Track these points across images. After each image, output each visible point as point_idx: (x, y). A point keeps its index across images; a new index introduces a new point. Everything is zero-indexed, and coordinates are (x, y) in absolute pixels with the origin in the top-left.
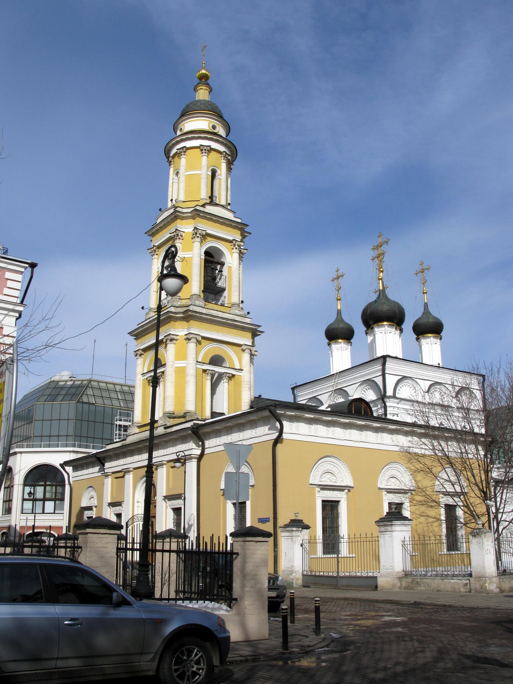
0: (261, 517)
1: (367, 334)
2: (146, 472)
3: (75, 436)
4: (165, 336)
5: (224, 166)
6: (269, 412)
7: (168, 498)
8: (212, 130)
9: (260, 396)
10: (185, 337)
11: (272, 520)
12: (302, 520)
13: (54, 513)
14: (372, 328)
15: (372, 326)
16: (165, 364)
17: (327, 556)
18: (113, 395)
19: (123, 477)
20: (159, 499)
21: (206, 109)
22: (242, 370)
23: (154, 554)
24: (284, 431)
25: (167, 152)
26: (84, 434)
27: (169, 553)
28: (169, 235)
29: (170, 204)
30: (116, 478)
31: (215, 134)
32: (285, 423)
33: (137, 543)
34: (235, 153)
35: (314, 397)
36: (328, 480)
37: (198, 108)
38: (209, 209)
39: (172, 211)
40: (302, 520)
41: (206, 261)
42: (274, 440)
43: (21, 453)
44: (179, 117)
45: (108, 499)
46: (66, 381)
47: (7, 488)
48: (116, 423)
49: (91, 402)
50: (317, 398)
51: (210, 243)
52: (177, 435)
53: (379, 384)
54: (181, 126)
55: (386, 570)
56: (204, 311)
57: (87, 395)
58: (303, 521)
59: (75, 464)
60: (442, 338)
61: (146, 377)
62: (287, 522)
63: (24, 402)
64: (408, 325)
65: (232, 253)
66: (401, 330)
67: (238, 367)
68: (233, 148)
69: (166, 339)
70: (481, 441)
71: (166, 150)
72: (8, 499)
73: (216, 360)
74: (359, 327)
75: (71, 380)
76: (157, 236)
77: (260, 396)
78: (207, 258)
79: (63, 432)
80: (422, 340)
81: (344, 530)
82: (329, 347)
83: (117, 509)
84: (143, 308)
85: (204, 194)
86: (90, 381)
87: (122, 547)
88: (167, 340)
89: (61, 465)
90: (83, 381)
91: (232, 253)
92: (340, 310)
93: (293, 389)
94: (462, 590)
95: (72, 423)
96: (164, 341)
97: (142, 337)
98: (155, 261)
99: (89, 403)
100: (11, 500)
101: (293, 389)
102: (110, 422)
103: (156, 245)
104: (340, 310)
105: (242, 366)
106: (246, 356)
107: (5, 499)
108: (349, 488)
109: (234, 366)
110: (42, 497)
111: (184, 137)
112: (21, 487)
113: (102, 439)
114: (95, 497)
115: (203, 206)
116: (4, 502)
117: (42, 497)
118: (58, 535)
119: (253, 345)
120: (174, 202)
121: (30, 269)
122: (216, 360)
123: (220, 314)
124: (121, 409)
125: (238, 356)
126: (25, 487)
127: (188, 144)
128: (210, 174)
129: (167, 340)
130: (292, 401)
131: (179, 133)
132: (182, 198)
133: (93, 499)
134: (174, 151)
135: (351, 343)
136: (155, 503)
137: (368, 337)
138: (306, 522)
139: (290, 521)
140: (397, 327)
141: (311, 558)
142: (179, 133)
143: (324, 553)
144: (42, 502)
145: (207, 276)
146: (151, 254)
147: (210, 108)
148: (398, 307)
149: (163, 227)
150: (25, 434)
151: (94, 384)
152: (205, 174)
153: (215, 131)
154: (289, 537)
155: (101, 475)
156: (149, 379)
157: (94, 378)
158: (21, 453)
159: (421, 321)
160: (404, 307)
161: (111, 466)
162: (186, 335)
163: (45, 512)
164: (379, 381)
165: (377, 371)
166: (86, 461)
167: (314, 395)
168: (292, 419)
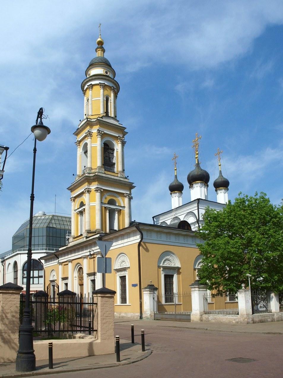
0: (133, 284)
1: (190, 188)
3: (47, 244)
4: (85, 189)
5: (112, 95)
7: (89, 275)
8: (105, 74)
9: (135, 221)
10: (95, 189)
11: (138, 285)
12: (154, 285)
13: (38, 284)
14: (193, 184)
16: (85, 204)
18: (65, 223)
19: (68, 264)
22: (125, 207)
23: (47, 304)
25: (82, 87)
26: (51, 243)
28: (85, 134)
29: (85, 117)
30: (64, 265)
33: (57, 298)
34: (119, 87)
35: (164, 222)
36: (168, 264)
38: (105, 120)
39: (86, 120)
40: (154, 285)
42: (138, 243)
43: (20, 254)
45: (61, 276)
47: (15, 272)
48: (67, 237)
51: (106, 139)
52: (92, 241)
54: (89, 72)
55: (195, 311)
56: (104, 175)
57: (52, 223)
58: (154, 286)
61: (76, 212)
62: (146, 286)
63: (21, 228)
64: (211, 183)
65: (118, 144)
66: (208, 186)
67: (122, 205)
69: (85, 191)
72: (16, 277)
74: (186, 184)
75: (44, 216)
77: (135, 221)
78: (105, 146)
81: (175, 290)
82: (171, 195)
83: (66, 281)
84: (73, 175)
86: (53, 216)
87: (57, 302)
89: (39, 259)
90: (49, 216)
91: (118, 144)
92: (176, 175)
93: (153, 218)
94: (234, 322)
95: (45, 238)
96: (84, 192)
97: (74, 191)
98: (78, 149)
99: (53, 228)
100: (17, 278)
101: (153, 218)
103: (79, 140)
104: (176, 175)
106: (126, 200)
107: (15, 278)
108: (179, 269)
109: (121, 204)
110: (34, 279)
111: (90, 79)
112: (21, 271)
113: (56, 245)
114: (55, 275)
115: (102, 118)
116: (14, 279)
117: (34, 279)
118: (233, 298)
119: (130, 194)
120: (87, 115)
121: (5, 151)
122: (112, 202)
123: (113, 177)
125: (122, 200)
126: (94, 279)
127: (93, 83)
128: (105, 99)
130: (153, 224)
132: (90, 113)
133: (55, 276)
134: (86, 87)
135: (182, 193)
136: (83, 277)
137: (191, 189)
138: (156, 286)
140: (205, 184)
141: (225, 303)
144: (37, 279)
146: (77, 145)
147: (104, 61)
148: (205, 172)
150: (22, 245)
151: (56, 218)
152: (101, 99)
153: (108, 75)
154: (147, 294)
156: (78, 213)
158: (20, 254)
160: (209, 173)
162: (95, 188)
163: (34, 283)
164: (196, 212)
165: (195, 207)
167: (164, 221)
168: (148, 231)
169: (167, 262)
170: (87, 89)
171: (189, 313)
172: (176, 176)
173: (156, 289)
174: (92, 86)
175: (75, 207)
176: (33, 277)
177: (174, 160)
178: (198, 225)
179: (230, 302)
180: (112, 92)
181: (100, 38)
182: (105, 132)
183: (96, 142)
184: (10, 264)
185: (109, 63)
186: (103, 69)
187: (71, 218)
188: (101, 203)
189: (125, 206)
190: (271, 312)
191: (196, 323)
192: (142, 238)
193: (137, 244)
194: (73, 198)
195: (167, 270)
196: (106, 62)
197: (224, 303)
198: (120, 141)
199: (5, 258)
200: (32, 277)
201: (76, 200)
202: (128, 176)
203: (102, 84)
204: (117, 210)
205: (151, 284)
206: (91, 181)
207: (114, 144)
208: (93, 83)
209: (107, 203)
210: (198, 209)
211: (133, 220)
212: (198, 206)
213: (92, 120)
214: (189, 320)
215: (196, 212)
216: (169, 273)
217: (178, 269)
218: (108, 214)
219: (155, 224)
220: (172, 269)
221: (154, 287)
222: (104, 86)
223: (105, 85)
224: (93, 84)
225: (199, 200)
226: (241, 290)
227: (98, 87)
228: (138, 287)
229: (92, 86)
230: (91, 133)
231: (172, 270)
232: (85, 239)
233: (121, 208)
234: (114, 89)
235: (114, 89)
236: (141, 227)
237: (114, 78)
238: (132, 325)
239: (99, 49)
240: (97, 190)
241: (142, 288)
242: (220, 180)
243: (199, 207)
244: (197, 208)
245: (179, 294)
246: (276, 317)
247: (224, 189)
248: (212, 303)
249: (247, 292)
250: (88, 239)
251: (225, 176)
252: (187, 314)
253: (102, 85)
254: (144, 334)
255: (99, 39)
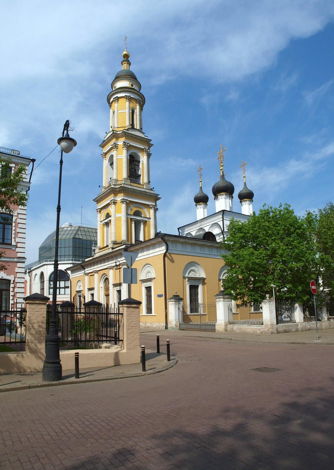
0: (159, 294)
1: (215, 199)
2: (58, 268)
4: (111, 201)
5: (138, 107)
6: (161, 239)
7: (115, 285)
9: (160, 232)
10: (121, 201)
12: (179, 296)
13: (65, 294)
14: (217, 196)
15: (217, 195)
16: (111, 216)
17: (256, 312)
19: (94, 275)
20: (111, 286)
21: (127, 74)
22: (151, 218)
24: (169, 249)
25: (108, 100)
27: (91, 312)
28: (111, 146)
29: (111, 129)
31: (133, 89)
32: (170, 245)
36: (193, 275)
37: (123, 74)
39: (112, 132)
40: (179, 296)
41: (130, 160)
43: (47, 265)
44: (114, 79)
45: (87, 287)
46: (67, 228)
48: (93, 248)
49: (80, 238)
50: (190, 233)
51: (132, 151)
53: (221, 226)
56: (130, 187)
59: (71, 269)
60: (253, 201)
61: (102, 223)
66: (232, 197)
67: (148, 216)
68: (143, 97)
70: (318, 265)
71: (108, 98)
73: (137, 213)
74: (211, 196)
75: (70, 227)
76: (105, 148)
77: (160, 232)
79: (67, 254)
80: (243, 202)
81: (200, 301)
83: (92, 292)
84: (99, 186)
85: (127, 124)
88: (111, 203)
90: (76, 227)
91: (143, 156)
92: (201, 187)
93: (178, 229)
95: (71, 249)
98: (104, 161)
99: (79, 239)
101: (178, 229)
102: (90, 248)
104: (201, 187)
105: (151, 216)
107: (41, 288)
108: (204, 279)
110: (61, 289)
111: (116, 91)
112: (48, 282)
114: (82, 286)
115: (127, 130)
116: (41, 289)
117: (61, 289)
118: (258, 308)
119: (156, 205)
120: (113, 127)
121: (32, 163)
122: (137, 213)
123: (138, 189)
124: (95, 241)
125: (148, 211)
127: (119, 95)
128: (131, 112)
129: (111, 203)
131: (114, 89)
132: (116, 126)
134: (112, 99)
135: (207, 204)
136: (109, 288)
138: (181, 296)
139: (172, 296)
140: (230, 195)
142: (114, 89)
143: (191, 312)
145: (132, 168)
147: (130, 74)
149: (108, 142)
151: (82, 229)
152: (127, 111)
153: (133, 87)
155: (83, 274)
156: (104, 224)
157: (83, 226)
158: (47, 265)
159: (241, 193)
161: (88, 270)
162: (121, 200)
164: (221, 223)
166: (74, 268)
167: (189, 232)
168: (173, 242)
169: (192, 273)
170: (113, 101)
171: (214, 323)
172: (201, 188)
173: (181, 299)
174: (118, 98)
175: (101, 218)
176: (60, 288)
177: (199, 171)
178: (222, 236)
179: (254, 312)
180: (138, 104)
181: (126, 51)
182: (131, 144)
183: (122, 154)
184: (36, 274)
185: (135, 76)
186: (129, 82)
187: (97, 229)
188: (127, 214)
189: (151, 217)
190: (295, 322)
191: (221, 333)
192: (167, 249)
193: (163, 255)
194: (99, 209)
195: (192, 281)
196: (131, 74)
197: (249, 314)
198: (146, 153)
199: (32, 269)
200: (58, 288)
201: (102, 211)
202: (153, 188)
203: (128, 97)
204: (142, 221)
205: (176, 294)
206: (116, 192)
207: (140, 156)
208: (119, 95)
209: (133, 214)
210: (223, 220)
211: (158, 231)
212: (223, 218)
213: (118, 132)
214: (214, 330)
215: (221, 223)
216: (195, 283)
217: (203, 280)
218: (133, 225)
219: (180, 235)
220: (191, 279)
221: (179, 298)
222: (129, 99)
223: (131, 97)
224: (118, 97)
225: (223, 211)
226: (265, 301)
227: (124, 99)
228: (163, 298)
229: (118, 98)
230: (117, 145)
231: (197, 281)
232: (111, 250)
233: (146, 220)
234: (140, 102)
235: (140, 102)
236: (166, 238)
237: (140, 91)
238: (157, 335)
239: (124, 62)
240: (123, 201)
241: (167, 298)
242: (245, 192)
243: (224, 219)
244: (222, 219)
245: (204, 304)
246: (300, 327)
247: (249, 201)
248: (237, 313)
249: (272, 303)
250: (114, 250)
251: (249, 188)
252: (212, 324)
253: (128, 98)
254: (169, 344)
255: (125, 53)
